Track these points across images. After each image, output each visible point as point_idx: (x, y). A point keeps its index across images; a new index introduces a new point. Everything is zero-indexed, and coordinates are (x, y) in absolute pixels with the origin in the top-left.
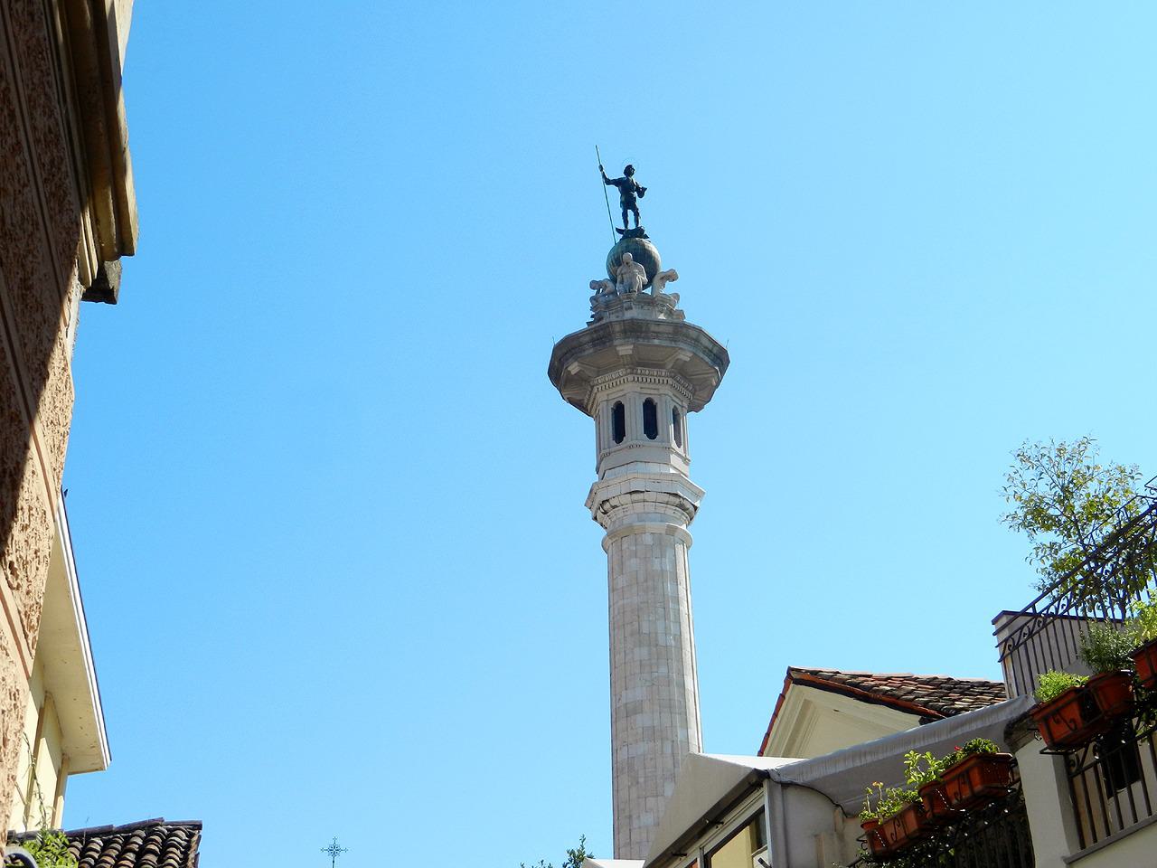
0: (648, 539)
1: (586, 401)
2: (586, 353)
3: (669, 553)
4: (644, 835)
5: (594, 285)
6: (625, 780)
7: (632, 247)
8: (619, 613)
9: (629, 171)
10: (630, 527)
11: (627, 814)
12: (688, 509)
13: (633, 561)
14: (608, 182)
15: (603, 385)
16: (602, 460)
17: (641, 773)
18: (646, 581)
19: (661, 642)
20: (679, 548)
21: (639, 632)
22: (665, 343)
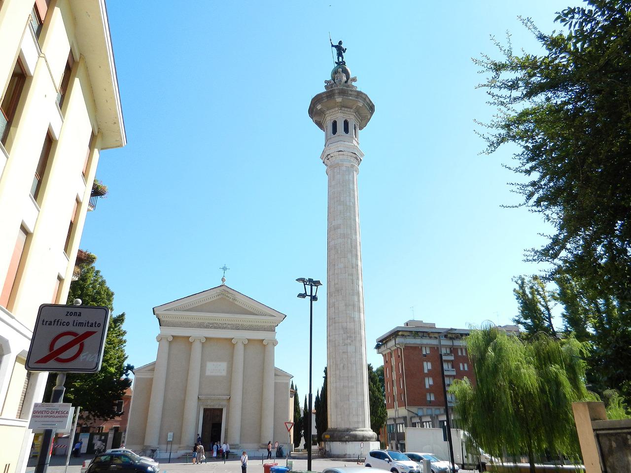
0: (344, 168)
5: (326, 82)
7: (341, 64)
9: (340, 43)
11: (333, 263)
14: (333, 46)
16: (327, 141)
19: (348, 204)
22: (354, 99)
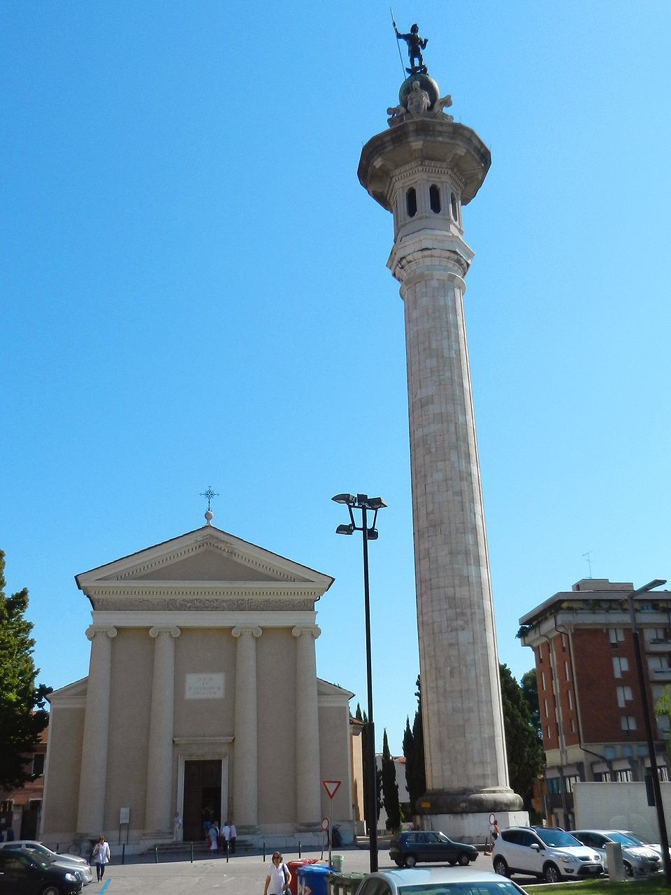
0: (435, 283)
1: (386, 192)
2: (388, 149)
3: (450, 294)
4: (436, 487)
7: (418, 80)
8: (457, 190)
9: (415, 29)
10: (422, 275)
11: (423, 473)
12: (463, 265)
14: (399, 36)
15: (405, 174)
18: (434, 313)
19: (446, 353)
20: (457, 291)
22: (447, 140)
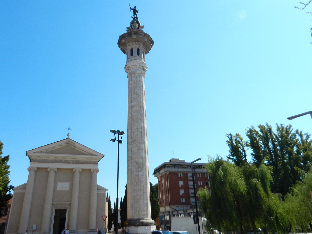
0: (137, 74)
3: (141, 77)
5: (127, 28)
6: (131, 120)
7: (135, 21)
9: (135, 7)
10: (134, 72)
11: (131, 126)
13: (134, 78)
14: (131, 9)
17: (134, 119)
19: (139, 94)
20: (143, 77)
21: (135, 92)
